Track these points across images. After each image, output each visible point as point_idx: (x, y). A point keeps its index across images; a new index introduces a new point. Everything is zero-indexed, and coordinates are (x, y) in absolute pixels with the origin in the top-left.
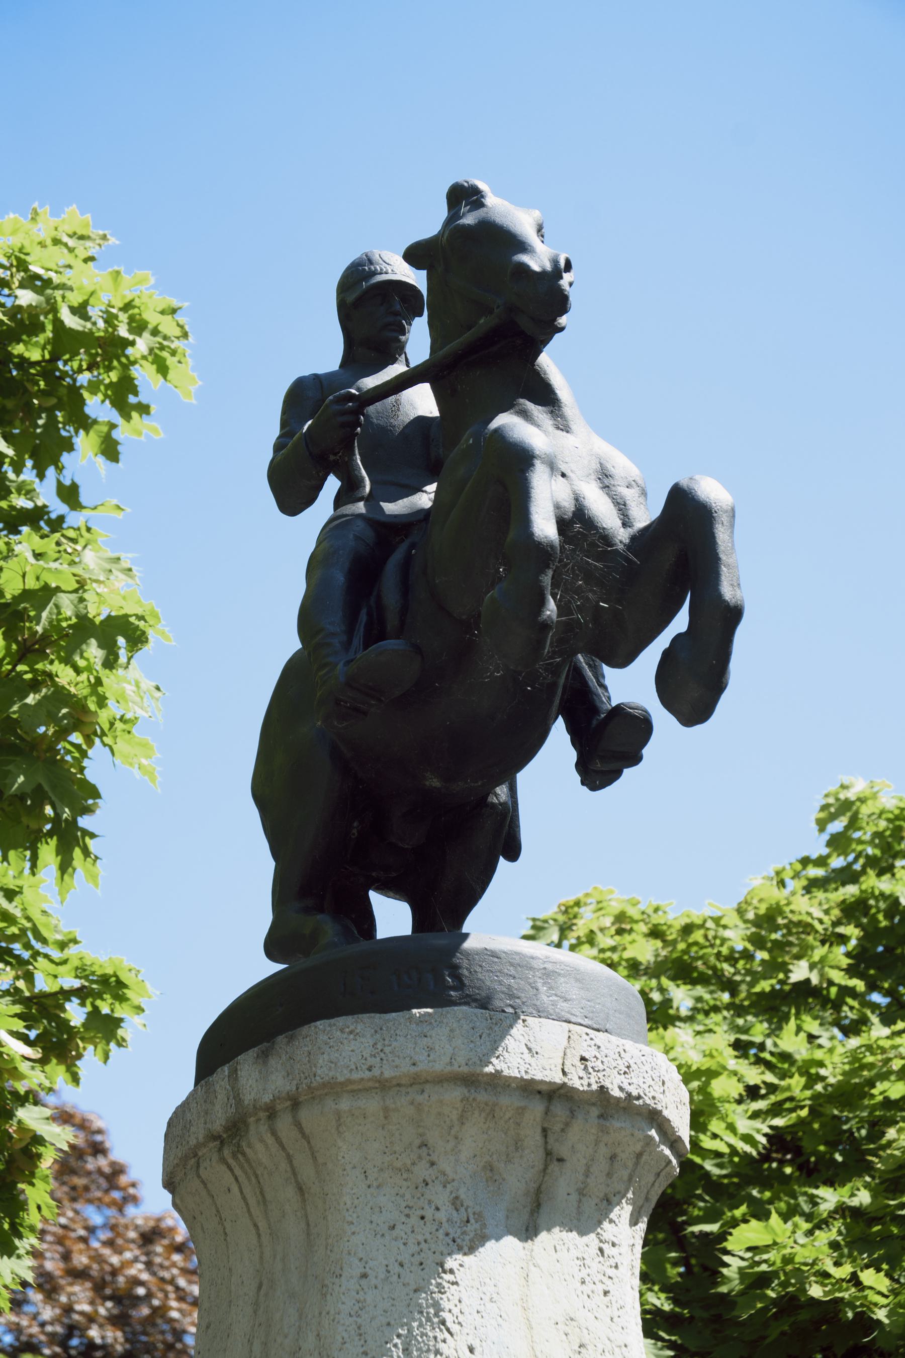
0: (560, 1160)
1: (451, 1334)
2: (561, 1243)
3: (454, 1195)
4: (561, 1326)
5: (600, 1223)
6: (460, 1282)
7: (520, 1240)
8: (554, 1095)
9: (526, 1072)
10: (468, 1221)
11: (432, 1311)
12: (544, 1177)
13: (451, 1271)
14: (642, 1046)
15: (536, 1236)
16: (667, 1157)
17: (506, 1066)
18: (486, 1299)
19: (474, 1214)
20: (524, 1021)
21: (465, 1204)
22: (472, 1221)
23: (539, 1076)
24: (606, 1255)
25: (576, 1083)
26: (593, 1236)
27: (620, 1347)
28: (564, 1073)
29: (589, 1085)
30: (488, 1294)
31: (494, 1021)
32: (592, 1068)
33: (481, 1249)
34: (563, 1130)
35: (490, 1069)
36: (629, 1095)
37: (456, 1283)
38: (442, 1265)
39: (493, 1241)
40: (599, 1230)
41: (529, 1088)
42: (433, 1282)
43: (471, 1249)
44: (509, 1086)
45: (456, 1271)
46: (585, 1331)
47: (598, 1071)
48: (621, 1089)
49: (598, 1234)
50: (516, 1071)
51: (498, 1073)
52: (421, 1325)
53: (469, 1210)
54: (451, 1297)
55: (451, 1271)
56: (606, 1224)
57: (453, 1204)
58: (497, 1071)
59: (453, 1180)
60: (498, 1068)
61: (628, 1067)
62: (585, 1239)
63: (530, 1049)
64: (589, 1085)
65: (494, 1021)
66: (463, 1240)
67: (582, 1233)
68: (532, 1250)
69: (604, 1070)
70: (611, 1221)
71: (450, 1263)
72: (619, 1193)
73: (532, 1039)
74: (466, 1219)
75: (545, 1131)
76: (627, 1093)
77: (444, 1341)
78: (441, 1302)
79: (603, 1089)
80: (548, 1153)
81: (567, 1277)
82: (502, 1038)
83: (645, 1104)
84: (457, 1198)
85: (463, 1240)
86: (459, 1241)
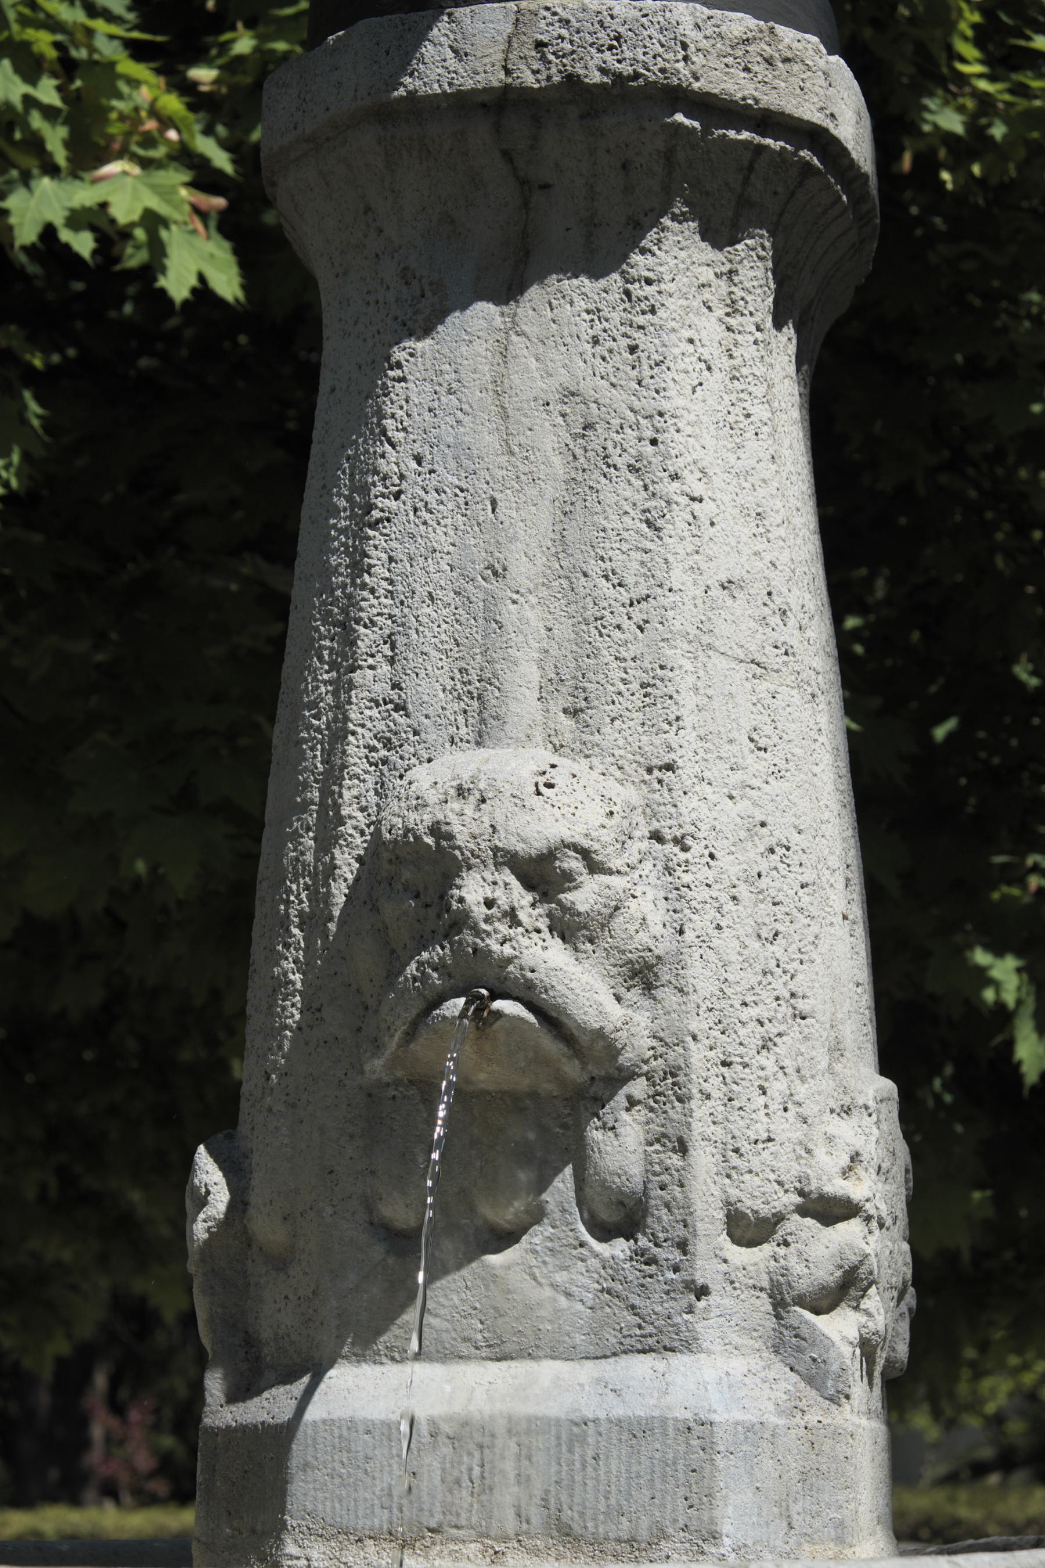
0: (545, 187)
1: (393, 445)
2: (559, 295)
3: (402, 266)
4: (555, 408)
5: (625, 257)
6: (409, 377)
7: (497, 303)
8: (502, 104)
9: (450, 84)
10: (423, 296)
11: (375, 420)
12: (527, 213)
13: (399, 365)
14: (420, 13)
15: (522, 294)
16: (746, 143)
17: (421, 83)
18: (442, 390)
19: (431, 284)
20: (450, 15)
21: (418, 275)
22: (428, 294)
23: (469, 84)
24: (634, 299)
25: (529, 80)
26: (616, 276)
27: (651, 417)
28: (508, 72)
29: (549, 78)
30: (445, 385)
31: (406, 27)
32: (554, 53)
33: (440, 328)
34: (532, 147)
35: (402, 92)
36: (618, 77)
37: (403, 379)
38: (388, 358)
39: (457, 314)
40: (624, 267)
41: (463, 104)
42: (380, 382)
43: (426, 331)
44: (438, 107)
45: (404, 363)
46: (594, 406)
47: (563, 56)
48: (603, 71)
49: (623, 272)
50: (436, 86)
51: (412, 94)
52: (365, 442)
53: (423, 281)
54: (395, 398)
55: (399, 365)
56: (636, 258)
57: (403, 278)
58: (409, 92)
59: (400, 247)
60: (411, 87)
61: (618, 38)
62: (602, 283)
63: (455, 51)
64: (549, 78)
65: (406, 27)
66: (416, 321)
67: (596, 275)
68: (515, 315)
69: (573, 52)
70: (644, 251)
71: (398, 354)
72: (652, 210)
73: (459, 37)
74: (419, 293)
75: (507, 155)
76: (614, 74)
77: (383, 456)
78: (384, 407)
79: (572, 80)
80: (524, 183)
81: (568, 340)
82: (417, 45)
83: (648, 83)
84: (406, 269)
85: (416, 321)
86: (409, 323)
